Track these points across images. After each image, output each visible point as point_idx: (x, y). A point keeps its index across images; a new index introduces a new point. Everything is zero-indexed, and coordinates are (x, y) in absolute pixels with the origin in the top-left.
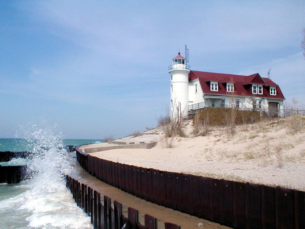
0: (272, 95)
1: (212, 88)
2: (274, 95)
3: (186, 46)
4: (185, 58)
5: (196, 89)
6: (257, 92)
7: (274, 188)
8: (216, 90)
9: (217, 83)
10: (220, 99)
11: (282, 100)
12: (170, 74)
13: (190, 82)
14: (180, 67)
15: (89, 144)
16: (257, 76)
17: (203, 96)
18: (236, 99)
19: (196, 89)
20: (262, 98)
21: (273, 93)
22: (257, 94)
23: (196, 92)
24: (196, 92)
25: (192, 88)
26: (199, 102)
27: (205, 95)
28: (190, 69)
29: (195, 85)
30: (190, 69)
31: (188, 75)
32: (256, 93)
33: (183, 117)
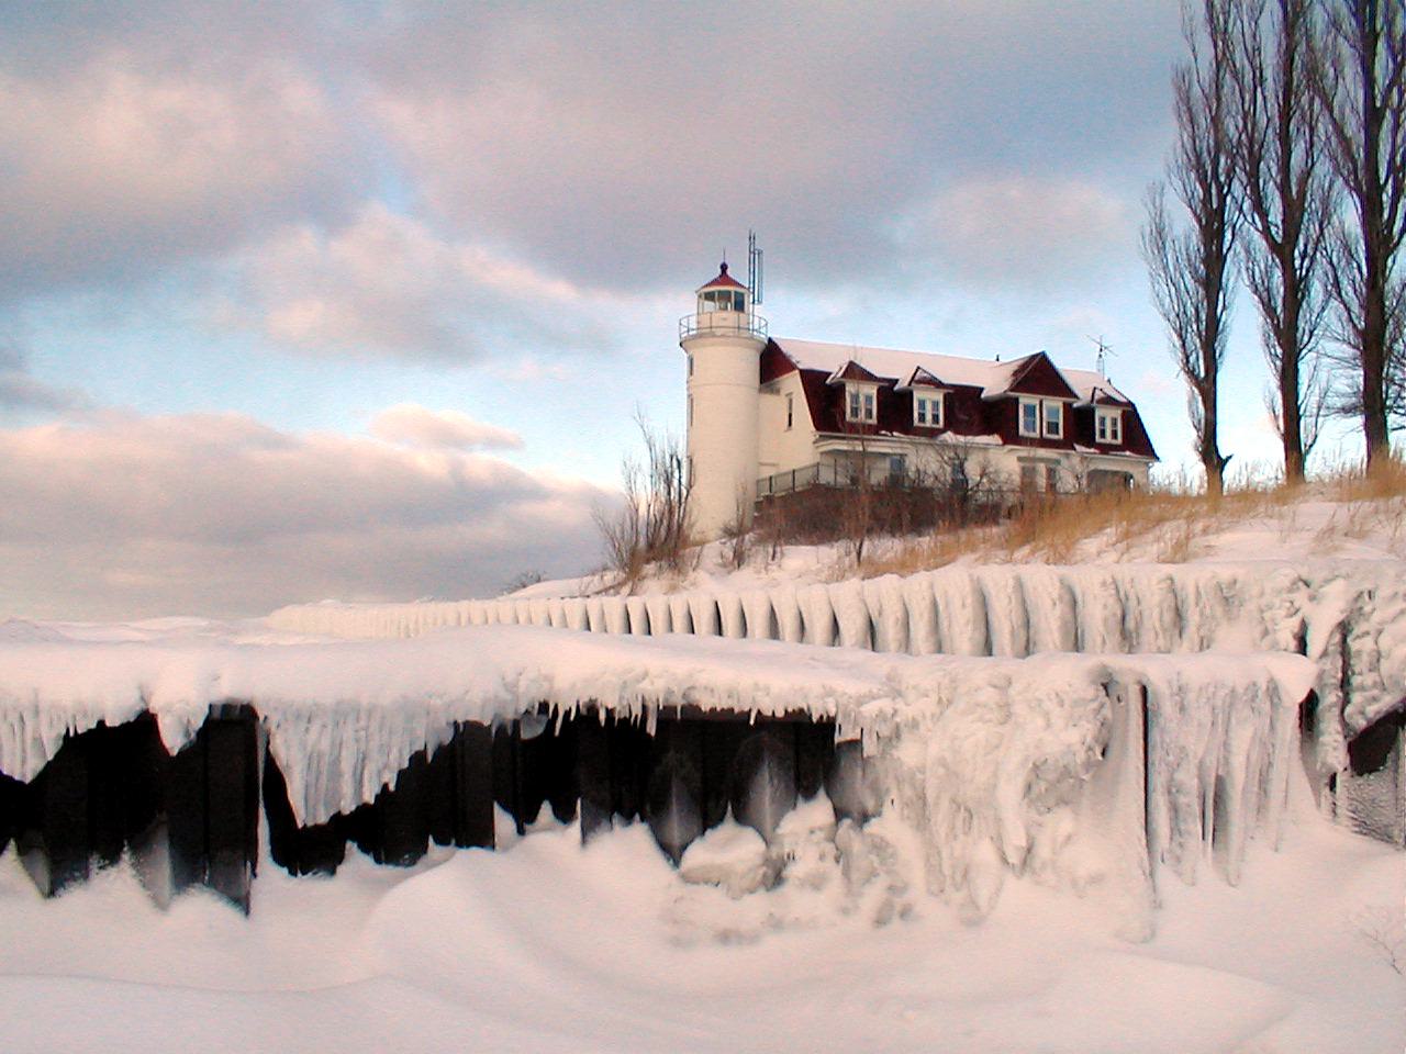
0: (1102, 441)
1: (919, 414)
2: (1114, 442)
3: (752, 238)
4: (747, 286)
5: (790, 416)
6: (1038, 431)
7: (188, 750)
8: (871, 418)
9: (875, 392)
10: (885, 455)
11: (1147, 464)
12: (686, 351)
13: (768, 383)
14: (724, 324)
15: (1075, 618)
16: (1039, 374)
17: (814, 443)
18: (1020, 459)
19: (790, 416)
20: (1060, 454)
21: (929, 417)
22: (1038, 436)
23: (790, 424)
24: (790, 424)
25: (774, 405)
26: (794, 467)
27: (821, 436)
28: (680, 329)
29: (787, 395)
30: (680, 329)
31: (756, 359)
32: (1036, 435)
33: (943, 521)
